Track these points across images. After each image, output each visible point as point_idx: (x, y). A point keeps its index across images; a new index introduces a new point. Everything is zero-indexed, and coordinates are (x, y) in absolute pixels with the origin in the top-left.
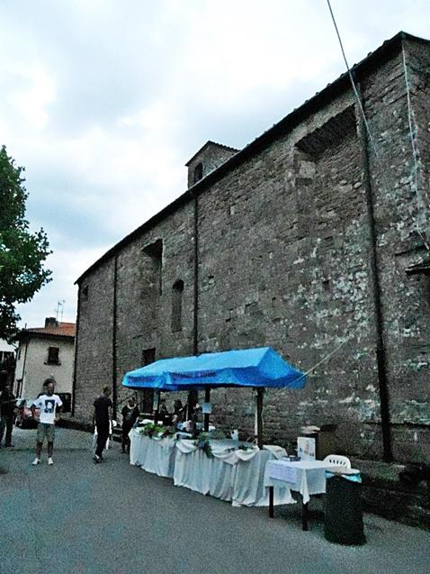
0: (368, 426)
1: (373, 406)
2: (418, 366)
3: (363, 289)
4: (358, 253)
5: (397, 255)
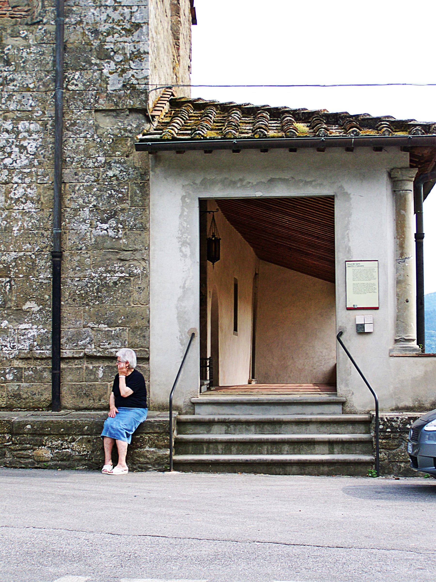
0: (17, 363)
1: (33, 332)
2: (115, 279)
3: (31, 148)
4: (28, 89)
5: (97, 111)
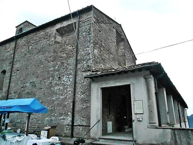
0: (67, 126)
4: (71, 69)
5: (82, 71)
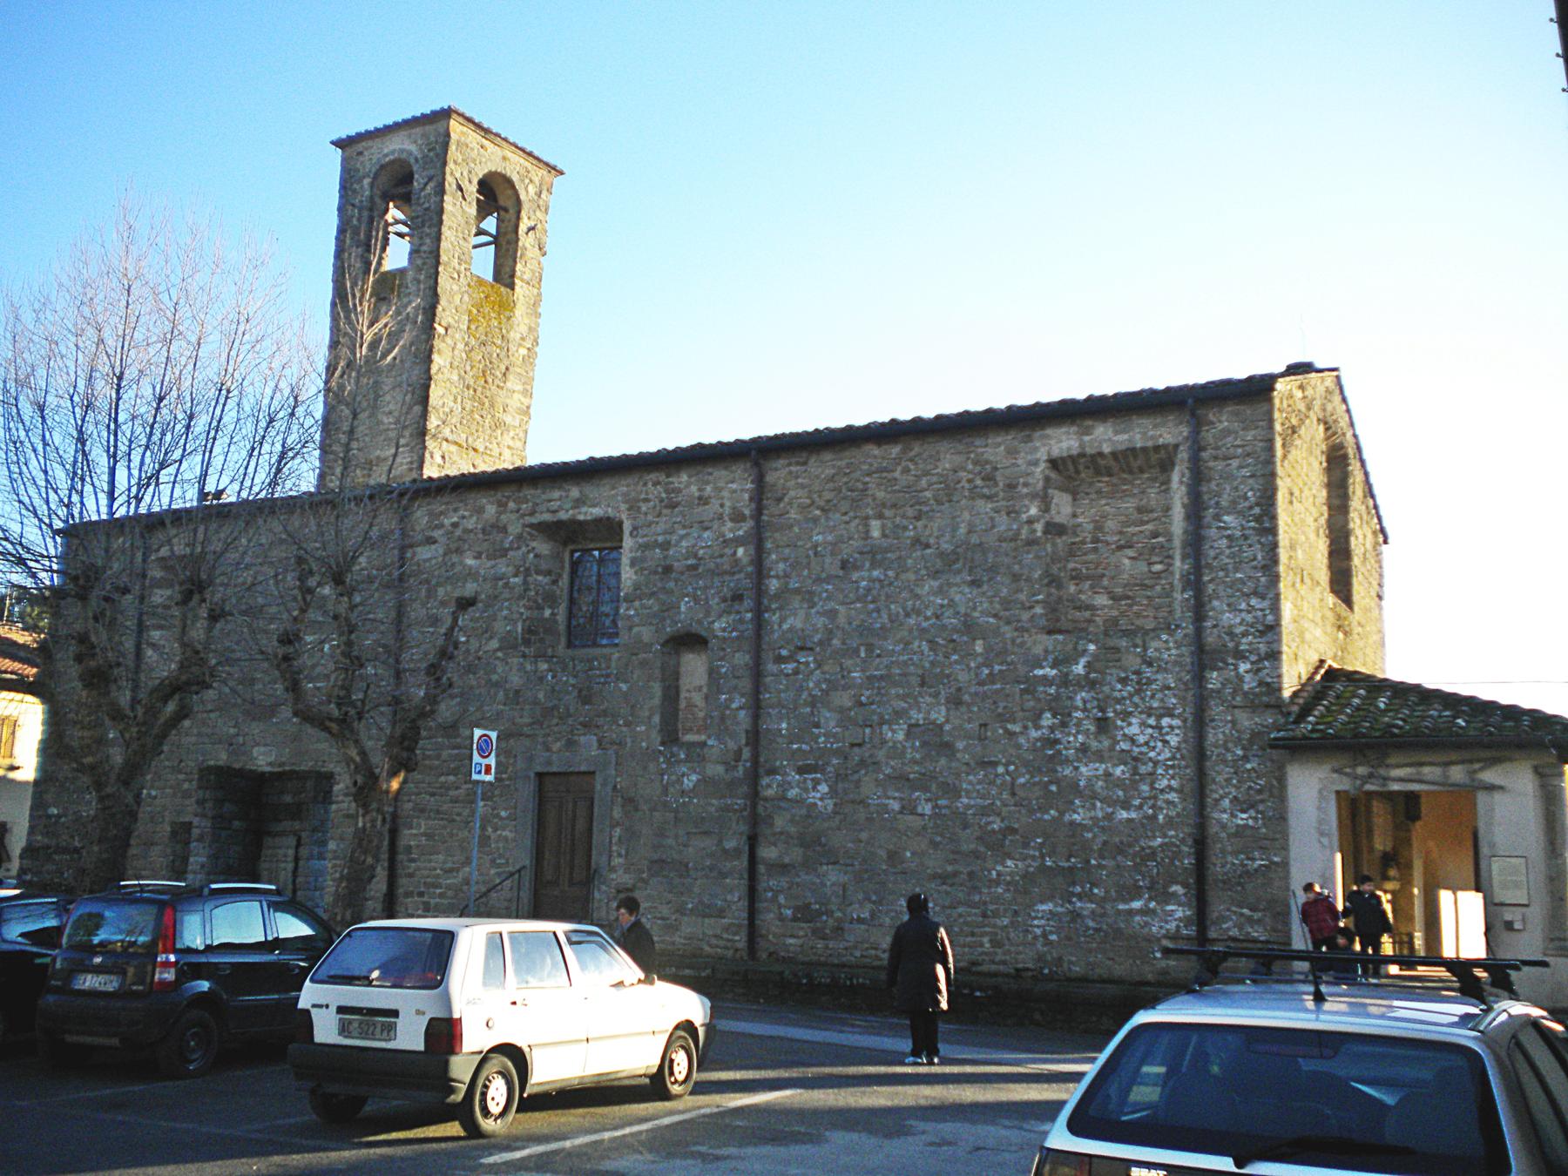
1: (1179, 914)
4: (1169, 688)
